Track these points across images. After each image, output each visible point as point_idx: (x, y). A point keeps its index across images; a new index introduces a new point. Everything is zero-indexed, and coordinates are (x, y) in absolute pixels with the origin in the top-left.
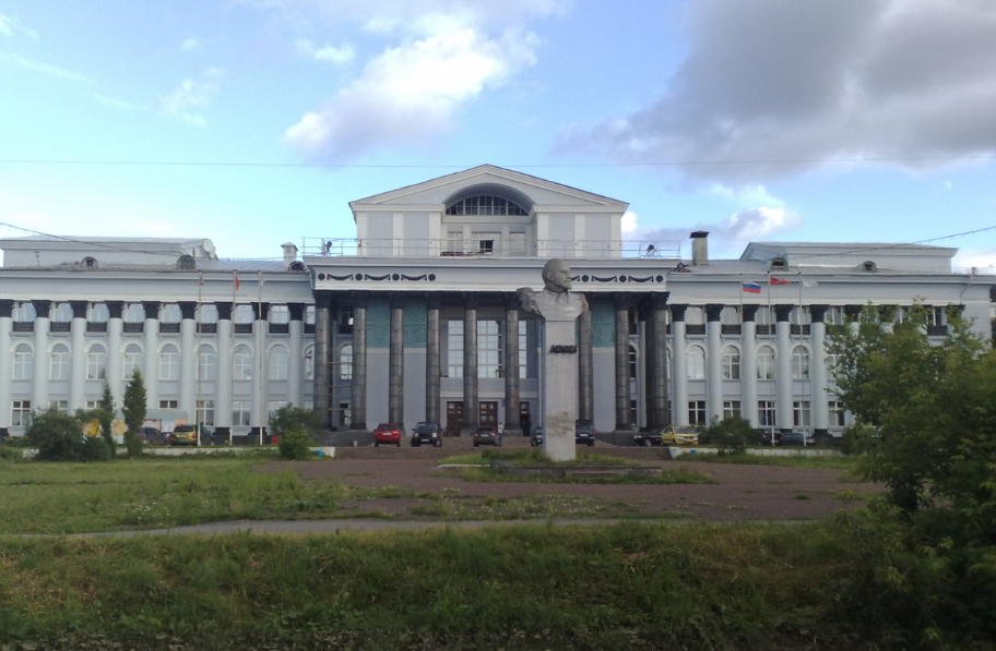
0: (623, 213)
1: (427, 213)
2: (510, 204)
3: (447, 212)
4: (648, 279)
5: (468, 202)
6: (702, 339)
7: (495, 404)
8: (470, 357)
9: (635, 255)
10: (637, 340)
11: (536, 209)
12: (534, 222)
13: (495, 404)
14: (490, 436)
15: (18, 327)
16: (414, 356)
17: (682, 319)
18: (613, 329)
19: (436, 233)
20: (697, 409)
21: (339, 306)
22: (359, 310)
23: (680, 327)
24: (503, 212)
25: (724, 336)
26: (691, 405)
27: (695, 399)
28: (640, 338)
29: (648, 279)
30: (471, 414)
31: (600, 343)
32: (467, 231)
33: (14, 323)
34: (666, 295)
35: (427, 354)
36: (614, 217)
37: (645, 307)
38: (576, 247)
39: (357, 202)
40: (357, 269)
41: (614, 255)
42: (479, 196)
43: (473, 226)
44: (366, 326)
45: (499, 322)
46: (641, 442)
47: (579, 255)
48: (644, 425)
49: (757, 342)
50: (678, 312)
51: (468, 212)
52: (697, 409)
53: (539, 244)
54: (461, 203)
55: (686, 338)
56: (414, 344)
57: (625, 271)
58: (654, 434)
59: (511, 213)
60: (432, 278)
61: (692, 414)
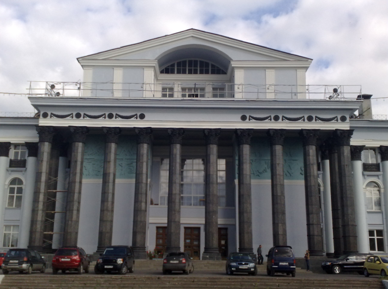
0: (307, 68)
1: (143, 67)
2: (213, 66)
3: (162, 72)
4: (333, 119)
5: (179, 64)
6: (378, 176)
7: (199, 229)
8: (174, 185)
9: (321, 97)
10: (381, 177)
11: (233, 64)
12: (231, 80)
13: (199, 229)
14: (181, 262)
15: (14, 164)
16: (123, 186)
17: (359, 158)
18: (302, 164)
19: (150, 85)
20: (376, 237)
21: (62, 141)
22: (76, 143)
23: (359, 165)
24: (207, 72)
25: (366, 173)
26: (371, 233)
27: (375, 228)
28: (384, 176)
29: (333, 119)
30: (311, 161)
31: (290, 176)
32: (177, 89)
33: (11, 160)
34: (349, 133)
35: (136, 184)
36: (300, 72)
37: (332, 145)
38: (267, 91)
39: (83, 58)
40: (77, 108)
41: (300, 97)
42: (187, 60)
43: (179, 81)
44: (82, 159)
45: (203, 160)
46: (329, 270)
47: (270, 96)
48: (332, 251)
49: (365, 178)
50: (356, 152)
51: (179, 72)
52: (376, 237)
53: (236, 87)
54: (173, 65)
55: (363, 175)
56: (259, 175)
57: (312, 111)
58: (342, 260)
59: (213, 73)
60: (142, 117)
61: (372, 241)
